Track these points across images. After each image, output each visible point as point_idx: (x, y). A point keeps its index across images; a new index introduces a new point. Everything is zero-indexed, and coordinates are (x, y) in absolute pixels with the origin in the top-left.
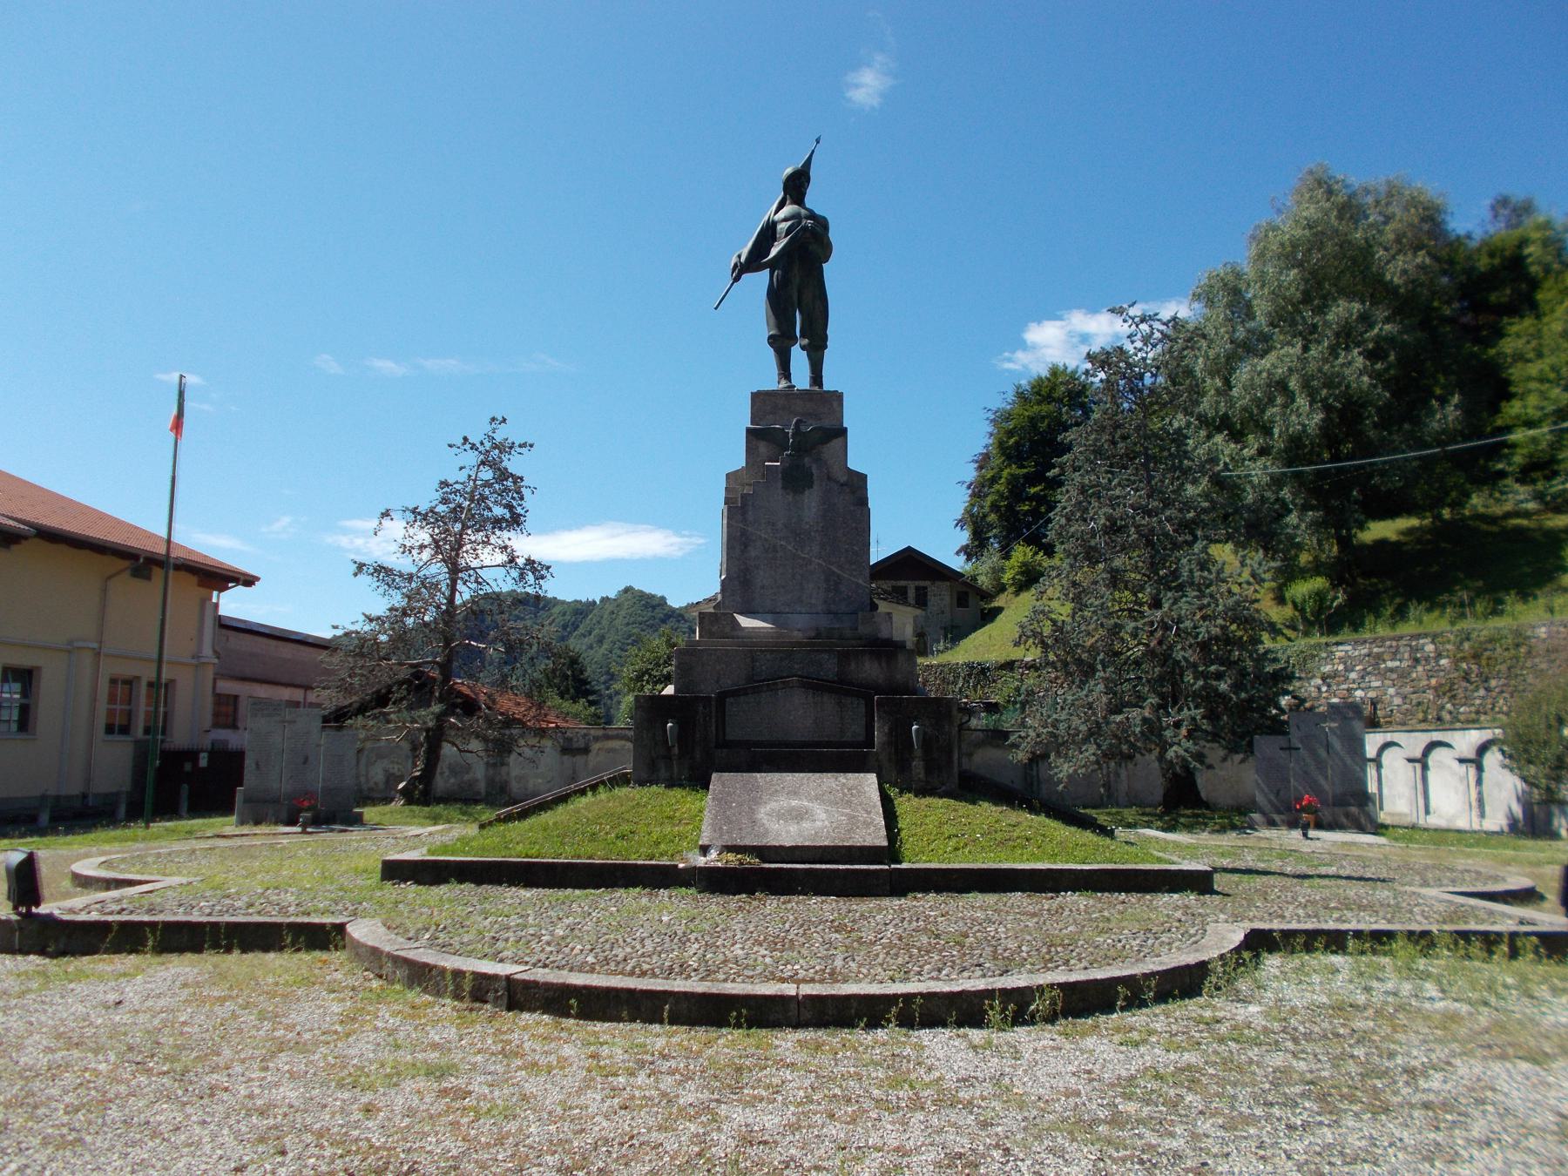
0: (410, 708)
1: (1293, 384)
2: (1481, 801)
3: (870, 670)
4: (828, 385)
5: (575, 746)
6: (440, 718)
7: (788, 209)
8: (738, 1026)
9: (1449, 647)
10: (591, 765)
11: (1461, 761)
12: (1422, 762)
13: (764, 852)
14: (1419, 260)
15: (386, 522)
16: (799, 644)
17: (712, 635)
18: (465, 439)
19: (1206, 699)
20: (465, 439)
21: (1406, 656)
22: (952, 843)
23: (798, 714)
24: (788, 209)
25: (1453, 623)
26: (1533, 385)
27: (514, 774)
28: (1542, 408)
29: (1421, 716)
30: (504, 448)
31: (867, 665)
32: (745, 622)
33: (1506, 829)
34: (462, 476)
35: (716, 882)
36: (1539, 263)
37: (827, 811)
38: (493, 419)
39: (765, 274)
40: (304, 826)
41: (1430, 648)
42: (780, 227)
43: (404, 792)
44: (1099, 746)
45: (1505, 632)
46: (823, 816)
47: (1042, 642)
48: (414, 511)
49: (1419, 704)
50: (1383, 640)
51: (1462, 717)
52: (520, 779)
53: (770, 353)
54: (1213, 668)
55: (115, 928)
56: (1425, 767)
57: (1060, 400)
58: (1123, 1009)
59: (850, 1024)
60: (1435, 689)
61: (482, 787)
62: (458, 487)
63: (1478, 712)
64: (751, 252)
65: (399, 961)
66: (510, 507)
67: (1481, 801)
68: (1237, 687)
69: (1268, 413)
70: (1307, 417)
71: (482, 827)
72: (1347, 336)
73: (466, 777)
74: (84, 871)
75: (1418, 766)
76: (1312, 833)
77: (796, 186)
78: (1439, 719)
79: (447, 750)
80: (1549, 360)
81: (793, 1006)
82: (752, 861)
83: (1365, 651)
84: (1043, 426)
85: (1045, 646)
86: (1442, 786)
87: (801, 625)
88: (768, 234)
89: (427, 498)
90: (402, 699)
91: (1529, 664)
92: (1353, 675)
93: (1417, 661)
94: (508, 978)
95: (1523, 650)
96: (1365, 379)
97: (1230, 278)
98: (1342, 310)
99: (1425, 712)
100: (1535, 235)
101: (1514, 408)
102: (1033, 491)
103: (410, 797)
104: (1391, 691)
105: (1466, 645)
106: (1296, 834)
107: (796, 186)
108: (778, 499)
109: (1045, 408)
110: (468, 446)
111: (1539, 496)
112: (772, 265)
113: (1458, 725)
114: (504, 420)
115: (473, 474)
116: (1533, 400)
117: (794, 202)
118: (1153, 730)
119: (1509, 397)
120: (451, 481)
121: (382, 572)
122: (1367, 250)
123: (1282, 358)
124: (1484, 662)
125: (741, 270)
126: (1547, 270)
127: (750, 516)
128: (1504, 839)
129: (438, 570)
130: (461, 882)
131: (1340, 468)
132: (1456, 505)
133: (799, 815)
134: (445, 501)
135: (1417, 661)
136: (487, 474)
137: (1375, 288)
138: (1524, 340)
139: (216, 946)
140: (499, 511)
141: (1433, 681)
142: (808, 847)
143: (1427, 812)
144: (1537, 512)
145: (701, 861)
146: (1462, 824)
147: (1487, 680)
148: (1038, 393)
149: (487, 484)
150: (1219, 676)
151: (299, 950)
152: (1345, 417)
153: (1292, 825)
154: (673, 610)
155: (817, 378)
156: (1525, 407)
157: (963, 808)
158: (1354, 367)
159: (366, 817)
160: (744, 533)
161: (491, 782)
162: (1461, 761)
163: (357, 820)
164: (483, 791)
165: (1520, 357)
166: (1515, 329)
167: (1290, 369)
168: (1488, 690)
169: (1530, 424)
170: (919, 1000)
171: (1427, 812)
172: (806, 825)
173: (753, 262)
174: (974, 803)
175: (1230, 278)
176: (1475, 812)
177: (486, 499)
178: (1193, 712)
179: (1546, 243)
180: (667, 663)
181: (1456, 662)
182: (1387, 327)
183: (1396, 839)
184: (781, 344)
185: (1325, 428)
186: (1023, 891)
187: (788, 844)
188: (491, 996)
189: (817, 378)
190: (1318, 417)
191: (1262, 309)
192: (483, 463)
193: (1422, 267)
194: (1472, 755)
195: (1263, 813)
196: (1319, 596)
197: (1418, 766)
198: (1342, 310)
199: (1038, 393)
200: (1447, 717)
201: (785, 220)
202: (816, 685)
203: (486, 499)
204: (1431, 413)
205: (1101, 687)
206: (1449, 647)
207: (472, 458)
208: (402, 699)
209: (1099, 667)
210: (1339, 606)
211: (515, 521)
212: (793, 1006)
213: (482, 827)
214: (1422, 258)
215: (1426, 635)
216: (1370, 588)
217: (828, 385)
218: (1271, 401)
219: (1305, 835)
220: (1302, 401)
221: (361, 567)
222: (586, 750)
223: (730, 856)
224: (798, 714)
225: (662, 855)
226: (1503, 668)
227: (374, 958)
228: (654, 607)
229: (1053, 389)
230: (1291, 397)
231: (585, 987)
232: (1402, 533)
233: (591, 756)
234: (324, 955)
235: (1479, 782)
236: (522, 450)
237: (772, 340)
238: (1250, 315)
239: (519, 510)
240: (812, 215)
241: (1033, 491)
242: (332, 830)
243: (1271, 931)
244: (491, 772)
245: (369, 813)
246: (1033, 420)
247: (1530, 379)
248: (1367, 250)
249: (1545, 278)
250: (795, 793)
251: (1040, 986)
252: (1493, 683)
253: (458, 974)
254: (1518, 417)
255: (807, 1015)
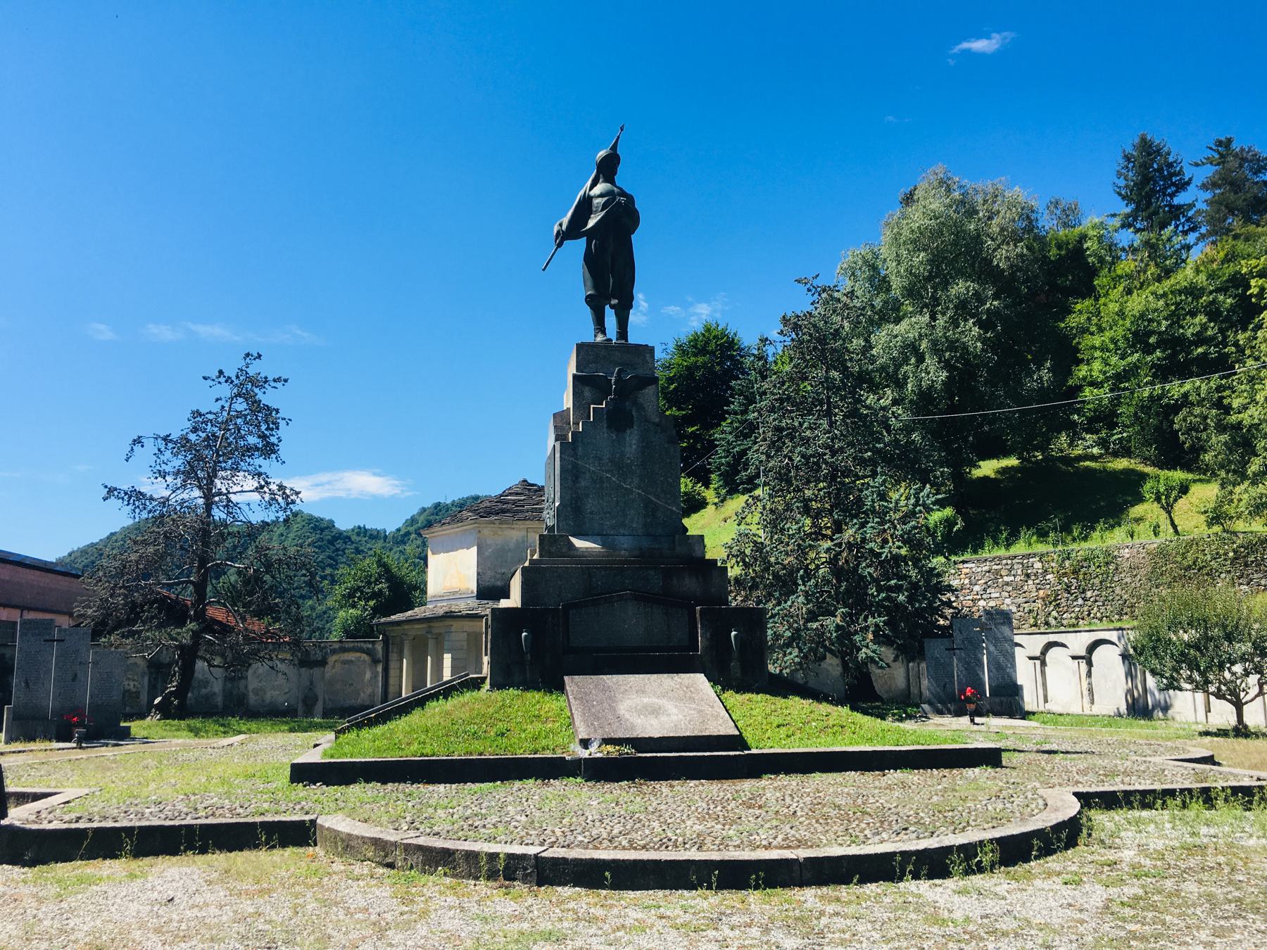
0: (160, 626)
1: (924, 345)
2: (1091, 691)
3: (690, 584)
4: (633, 339)
5: (312, 658)
6: (196, 635)
7: (601, 187)
8: (756, 888)
9: (1053, 564)
10: (327, 676)
11: (1074, 658)
12: (1041, 659)
13: (640, 743)
14: (1018, 250)
15: (137, 448)
16: (626, 562)
17: (550, 554)
18: (221, 372)
19: (888, 611)
20: (221, 372)
21: (1019, 572)
22: (783, 730)
23: (632, 623)
24: (601, 187)
25: (1055, 545)
26: (1098, 354)
27: (250, 687)
28: (1105, 373)
29: (1032, 621)
30: (254, 381)
31: (687, 581)
32: (579, 543)
33: (1123, 709)
34: (216, 408)
35: (599, 771)
36: (1096, 255)
37: (676, 707)
38: (248, 355)
39: (583, 241)
40: (79, 741)
41: (1038, 565)
42: (596, 201)
43: (158, 707)
44: (801, 650)
45: (1097, 552)
46: (675, 711)
47: (744, 561)
48: (166, 439)
49: (1030, 611)
50: (1000, 559)
51: (1065, 622)
52: (256, 692)
53: (587, 312)
54: (893, 582)
55: (90, 834)
56: (1043, 664)
57: (713, 353)
58: (1037, 858)
59: (846, 881)
60: (1043, 599)
61: (219, 700)
62: (211, 417)
63: (1077, 618)
64: (570, 222)
65: (409, 849)
66: (263, 437)
67: (1091, 691)
68: (911, 599)
69: (903, 371)
70: (934, 373)
71: (338, 732)
72: (964, 308)
73: (204, 691)
74: (65, 783)
75: (1038, 662)
76: (977, 720)
77: (607, 169)
78: (1047, 623)
79: (200, 665)
80: (1108, 334)
81: (796, 868)
82: (627, 750)
83: (986, 568)
84: (698, 374)
85: (746, 565)
86: (1071, 680)
87: (625, 543)
88: (585, 206)
89: (178, 426)
90: (152, 618)
91: (1116, 579)
92: (977, 588)
93: (1028, 576)
94: (536, 856)
95: (1112, 567)
96: (979, 344)
97: (870, 256)
98: (961, 288)
99: (1035, 618)
100: (1091, 233)
101: (1082, 371)
102: (690, 430)
103: (167, 712)
104: (1008, 601)
105: (1067, 563)
106: (965, 720)
107: (607, 169)
108: (604, 436)
109: (701, 359)
110: (222, 379)
111: (1103, 443)
112: (591, 234)
113: (1062, 629)
114: (259, 356)
115: (227, 405)
116: (1097, 365)
117: (605, 181)
118: (844, 634)
119: (1079, 362)
120: (203, 411)
121: (135, 496)
122: (977, 239)
123: (910, 327)
124: (1081, 577)
125: (564, 236)
126: (1101, 260)
127: (580, 450)
128: (1123, 721)
129: (195, 495)
130: (367, 781)
131: (959, 417)
132: (1044, 448)
133: (655, 711)
134: (195, 430)
135: (1028, 576)
136: (240, 405)
137: (985, 271)
138: (1085, 316)
139: (191, 847)
140: (252, 440)
141: (1041, 592)
142: (689, 737)
143: (1046, 701)
144: (1101, 456)
145: (584, 754)
146: (1076, 709)
147: (1084, 591)
148: (695, 347)
149: (240, 414)
150: (898, 589)
151: (273, 847)
152: (963, 371)
153: (959, 713)
154: (340, 533)
155: (623, 333)
156: (1091, 370)
157: (780, 702)
158: (971, 333)
159: (133, 731)
160: (575, 466)
161: (228, 695)
162: (1074, 658)
163: (125, 735)
164: (220, 704)
165: (1084, 331)
166: (1078, 307)
167: (920, 335)
168: (1085, 599)
169: (1094, 384)
170: (898, 858)
171: (1046, 701)
172: (663, 718)
173: (574, 230)
174: (785, 697)
175: (870, 256)
176: (1087, 699)
177: (237, 430)
178: (878, 620)
179: (1100, 238)
180: (377, 581)
181: (1060, 577)
182: (995, 303)
183: (1044, 722)
184: (596, 305)
185: (947, 384)
186: (856, 770)
187: (657, 736)
188: (519, 873)
189: (623, 333)
190: (944, 375)
191: (897, 284)
192: (239, 395)
193: (1021, 255)
194: (1083, 653)
195: (930, 703)
196: (949, 523)
197: (1038, 662)
198: (961, 288)
199: (695, 347)
200: (1053, 622)
201: (601, 196)
202: (644, 598)
203: (237, 430)
204: (1030, 374)
205: (801, 599)
206: (1053, 564)
207: (226, 390)
208: (152, 618)
209: (800, 582)
210: (958, 531)
211: (269, 450)
212: (796, 868)
213: (338, 732)
214: (1021, 248)
215: (1035, 555)
216: (987, 516)
217: (633, 339)
218: (906, 361)
219: (972, 721)
220: (930, 362)
221: (111, 491)
222: (323, 663)
223: (610, 748)
224: (632, 623)
225: (543, 749)
226: (1097, 581)
227: (347, 846)
228: (322, 530)
229: (707, 343)
230: (921, 359)
231: (614, 861)
232: (998, 472)
233: (328, 668)
234: (301, 850)
235: (1089, 674)
236: (278, 385)
237: (589, 300)
238: (888, 290)
239: (273, 440)
240: (623, 193)
241: (690, 430)
242: (107, 745)
243: (1115, 792)
244: (229, 685)
245: (136, 727)
246: (691, 369)
247: (1094, 348)
248: (977, 239)
249: (1101, 268)
250: (642, 691)
251: (981, 842)
252: (1089, 594)
253: (493, 857)
254: (1084, 378)
255: (807, 875)
